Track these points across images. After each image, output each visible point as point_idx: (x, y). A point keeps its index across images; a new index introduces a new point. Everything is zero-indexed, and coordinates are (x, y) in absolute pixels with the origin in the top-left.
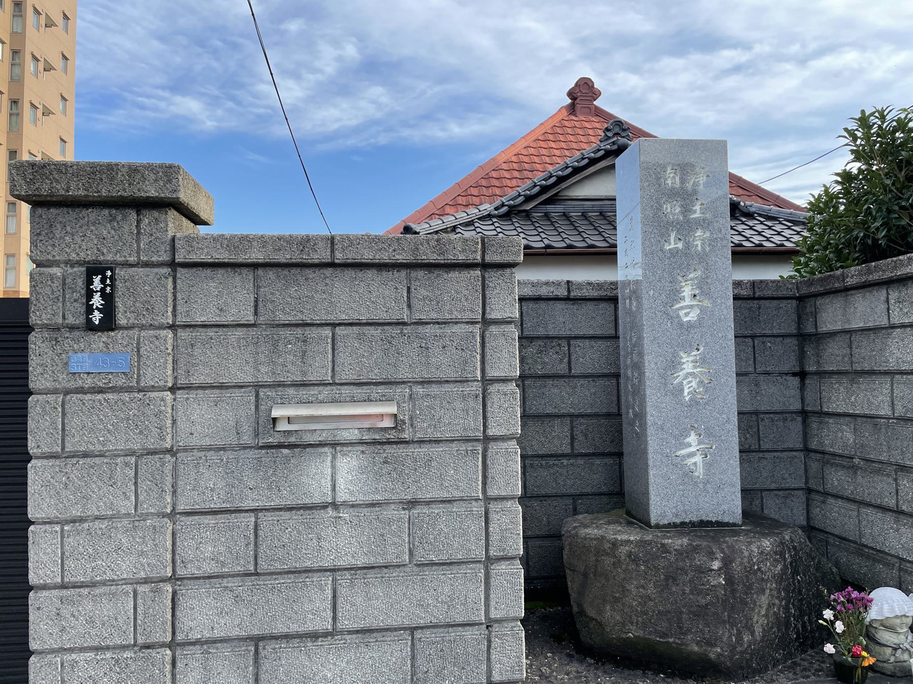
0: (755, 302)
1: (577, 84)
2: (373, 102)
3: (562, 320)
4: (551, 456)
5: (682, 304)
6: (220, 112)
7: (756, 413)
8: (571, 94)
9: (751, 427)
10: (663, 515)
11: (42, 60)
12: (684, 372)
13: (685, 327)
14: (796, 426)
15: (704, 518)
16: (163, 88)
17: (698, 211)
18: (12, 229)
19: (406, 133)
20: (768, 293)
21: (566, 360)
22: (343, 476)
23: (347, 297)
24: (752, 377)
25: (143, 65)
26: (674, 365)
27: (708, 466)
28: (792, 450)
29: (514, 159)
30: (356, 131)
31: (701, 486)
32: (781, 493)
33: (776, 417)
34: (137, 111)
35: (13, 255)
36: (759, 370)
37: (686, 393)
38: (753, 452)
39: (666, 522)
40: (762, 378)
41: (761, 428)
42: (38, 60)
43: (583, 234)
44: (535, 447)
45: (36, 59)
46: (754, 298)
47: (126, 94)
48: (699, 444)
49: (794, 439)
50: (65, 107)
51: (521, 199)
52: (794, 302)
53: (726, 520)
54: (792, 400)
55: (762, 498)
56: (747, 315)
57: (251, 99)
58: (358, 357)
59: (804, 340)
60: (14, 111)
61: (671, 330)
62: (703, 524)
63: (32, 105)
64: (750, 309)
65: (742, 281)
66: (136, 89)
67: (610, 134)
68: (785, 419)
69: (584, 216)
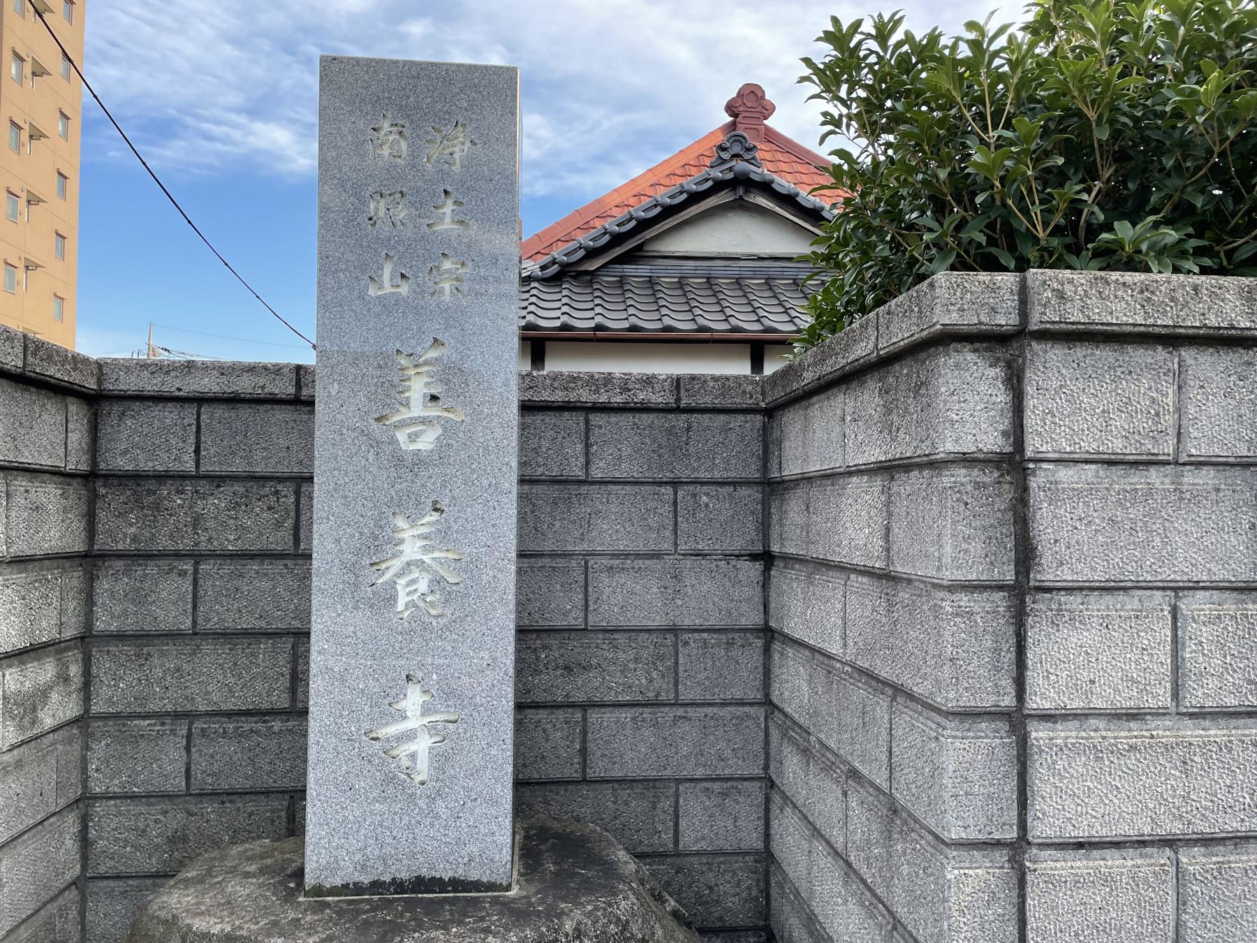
0: (684, 416)
1: (740, 94)
3: (283, 442)
4: (248, 713)
5: (405, 414)
7: (674, 630)
8: (731, 108)
9: (662, 658)
10: (333, 868)
11: (29, 60)
12: (405, 558)
13: (408, 462)
14: (750, 657)
15: (425, 872)
16: (238, 111)
17: (448, 219)
19: (573, 180)
20: (706, 400)
21: (289, 523)
24: (669, 560)
25: (210, 79)
26: (378, 544)
27: (441, 760)
28: (741, 703)
31: (422, 803)
32: (716, 786)
33: (712, 639)
34: (203, 143)
36: (682, 547)
37: (400, 606)
38: (665, 705)
39: (338, 882)
40: (688, 563)
41: (681, 661)
42: (22, 60)
43: (796, 320)
44: (215, 697)
45: (19, 58)
46: (678, 410)
47: (190, 121)
48: (423, 714)
49: (745, 685)
50: (66, 128)
51: (581, 253)
52: (759, 418)
53: (474, 876)
54: (744, 607)
55: (677, 796)
56: (664, 441)
59: (772, 492)
61: (374, 469)
62: (420, 884)
63: (13, 123)
64: (670, 431)
65: (654, 376)
66: (200, 112)
67: (725, 156)
68: (730, 644)
69: (681, 284)
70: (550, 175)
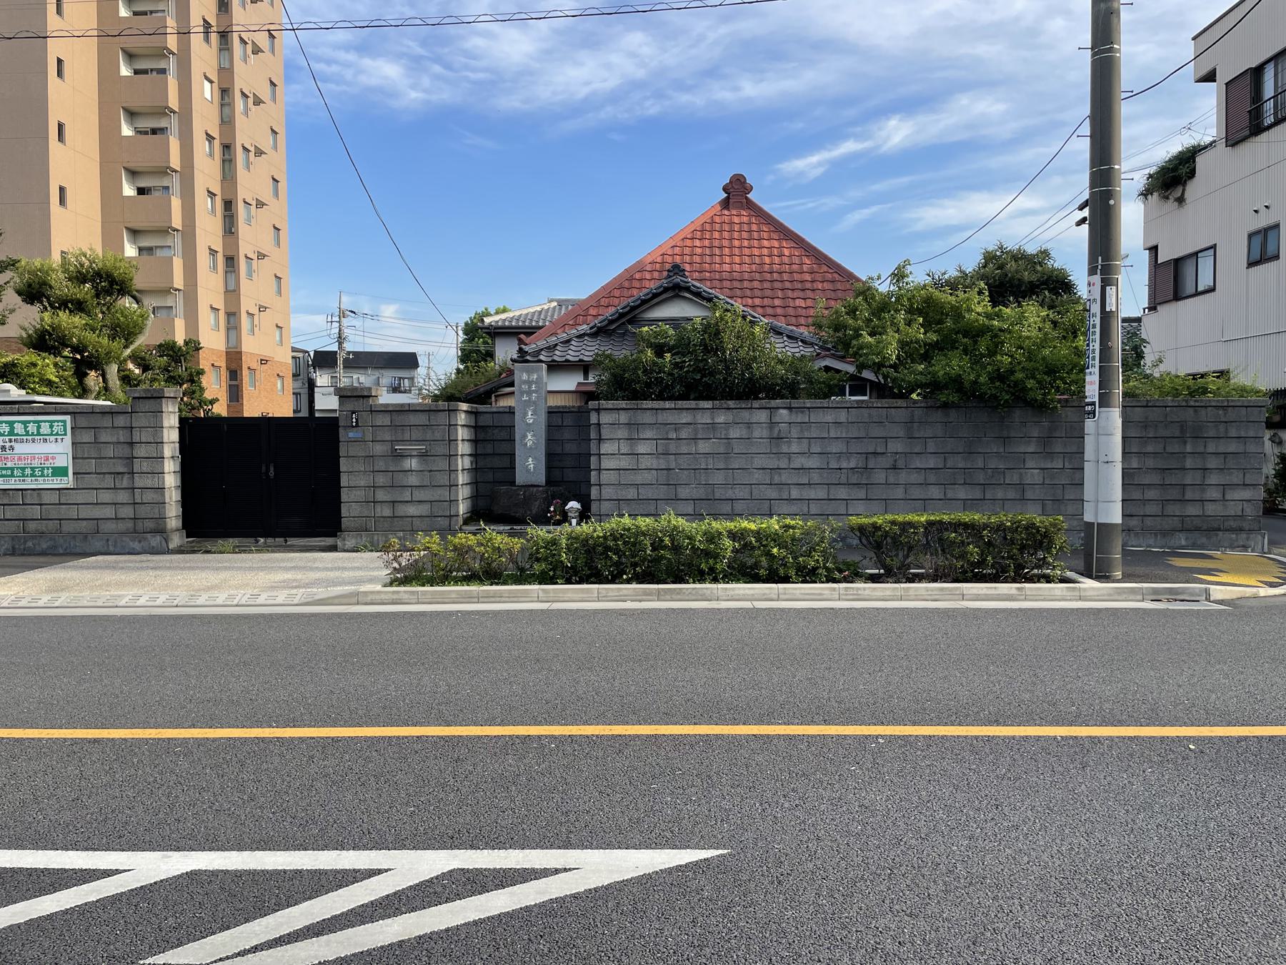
2: (632, 55)
6: (426, 81)
18: (231, 287)
19: (684, 98)
22: (413, 463)
23: (413, 419)
26: (525, 436)
29: (659, 260)
30: (614, 97)
35: (234, 314)
45: (244, 95)
57: (463, 60)
58: (416, 434)
60: (227, 157)
63: (244, 148)
70: (659, 95)
